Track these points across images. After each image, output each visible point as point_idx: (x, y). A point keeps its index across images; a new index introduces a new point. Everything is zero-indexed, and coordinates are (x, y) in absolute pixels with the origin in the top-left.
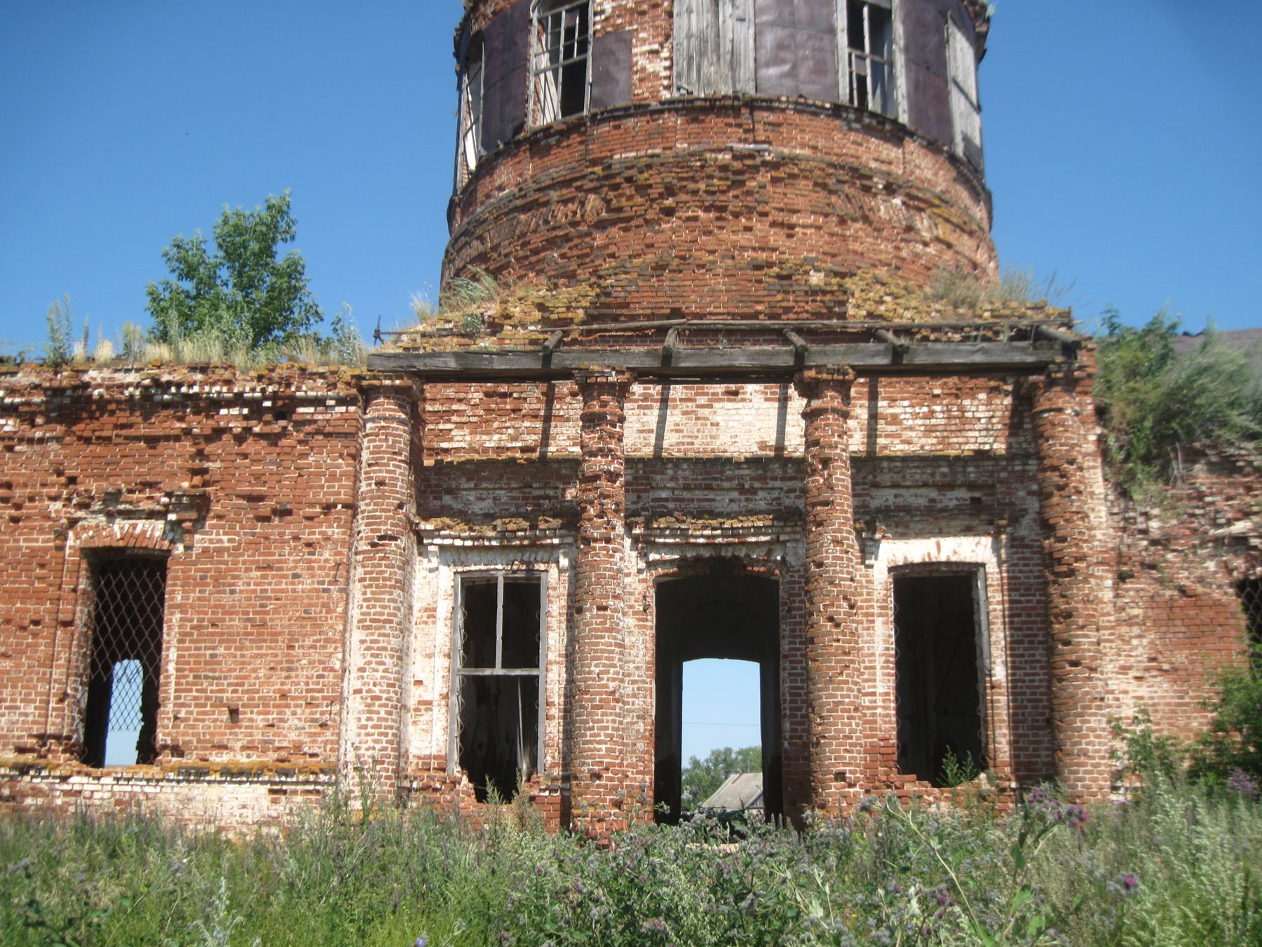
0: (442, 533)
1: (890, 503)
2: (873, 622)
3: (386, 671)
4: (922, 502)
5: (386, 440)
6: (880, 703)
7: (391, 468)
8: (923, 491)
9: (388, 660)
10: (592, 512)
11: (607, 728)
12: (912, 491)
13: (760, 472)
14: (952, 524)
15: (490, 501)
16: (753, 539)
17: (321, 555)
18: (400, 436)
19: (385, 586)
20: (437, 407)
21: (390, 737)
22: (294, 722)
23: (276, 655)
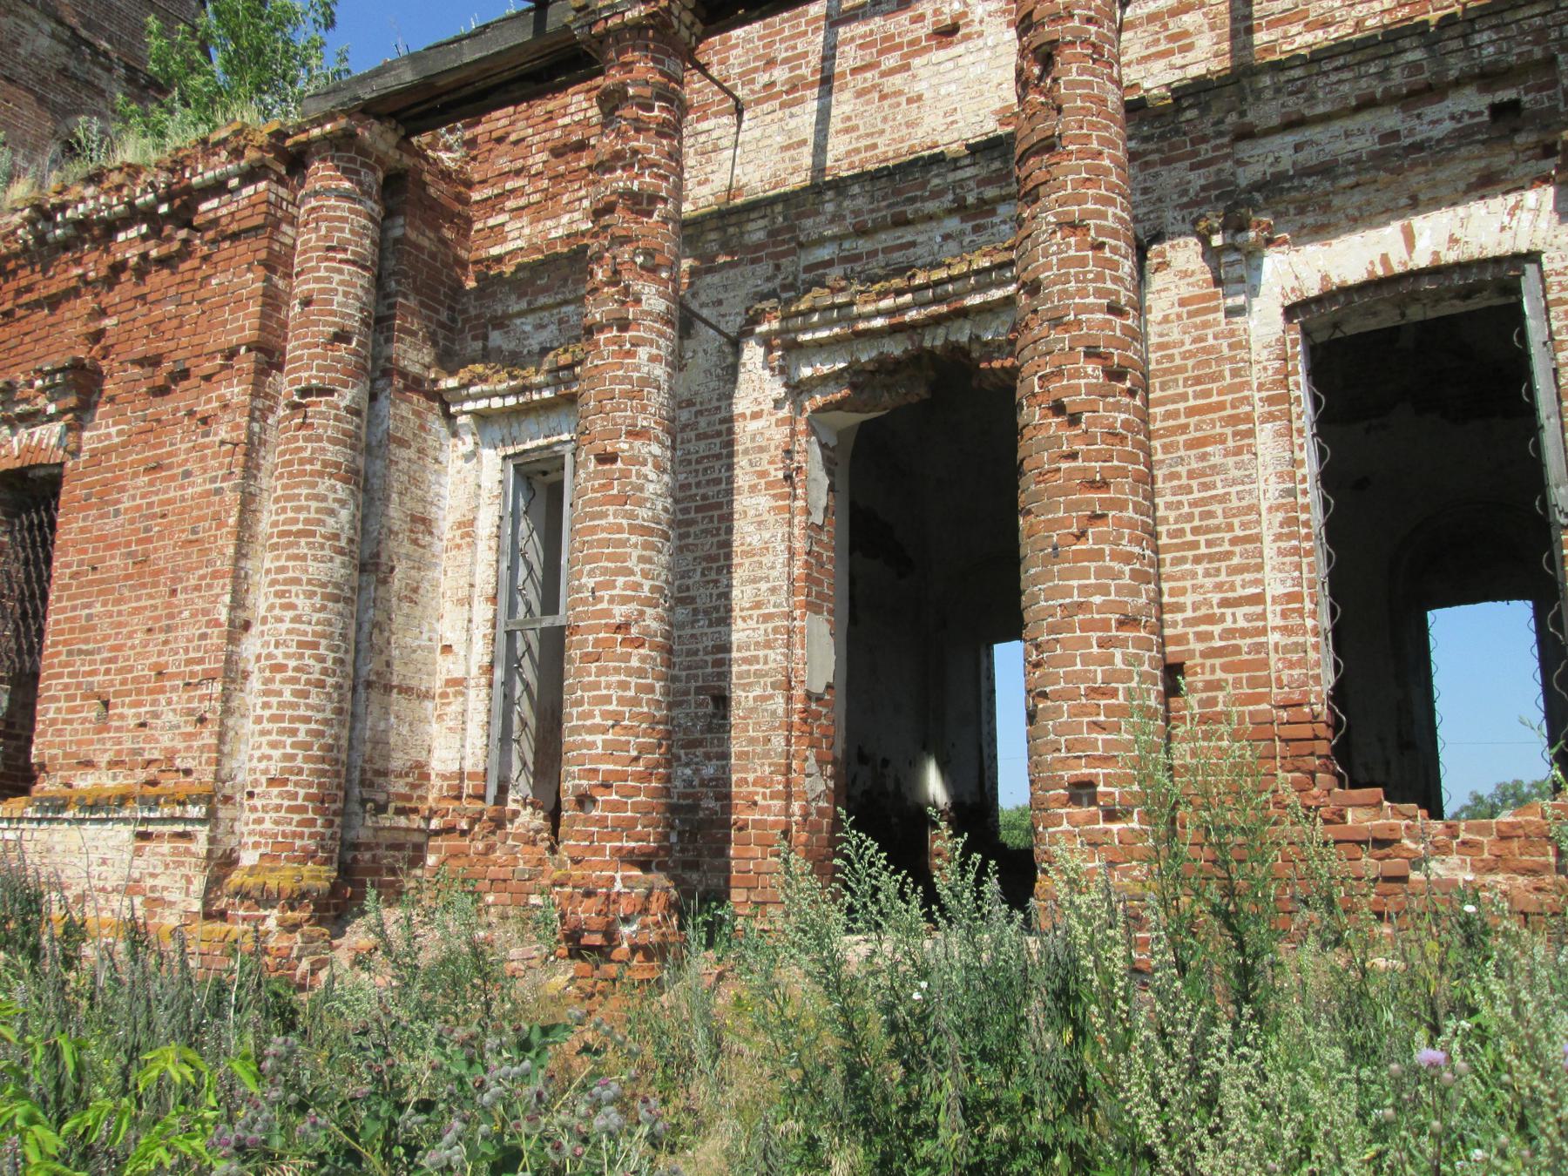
0: (473, 390)
1: (1286, 165)
2: (1251, 433)
3: (297, 619)
4: (1365, 144)
5: (317, 229)
6: (1274, 620)
7: (322, 274)
8: (1366, 119)
9: (301, 602)
10: (600, 275)
11: (607, 700)
12: (1337, 126)
13: (996, 165)
14: (1442, 175)
15: (553, 327)
16: (976, 300)
17: (216, 434)
18: (343, 219)
19: (303, 473)
20: (487, 192)
21: (302, 736)
22: (169, 717)
23: (155, 608)
